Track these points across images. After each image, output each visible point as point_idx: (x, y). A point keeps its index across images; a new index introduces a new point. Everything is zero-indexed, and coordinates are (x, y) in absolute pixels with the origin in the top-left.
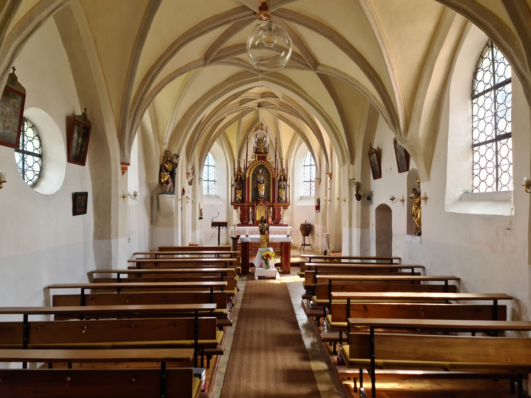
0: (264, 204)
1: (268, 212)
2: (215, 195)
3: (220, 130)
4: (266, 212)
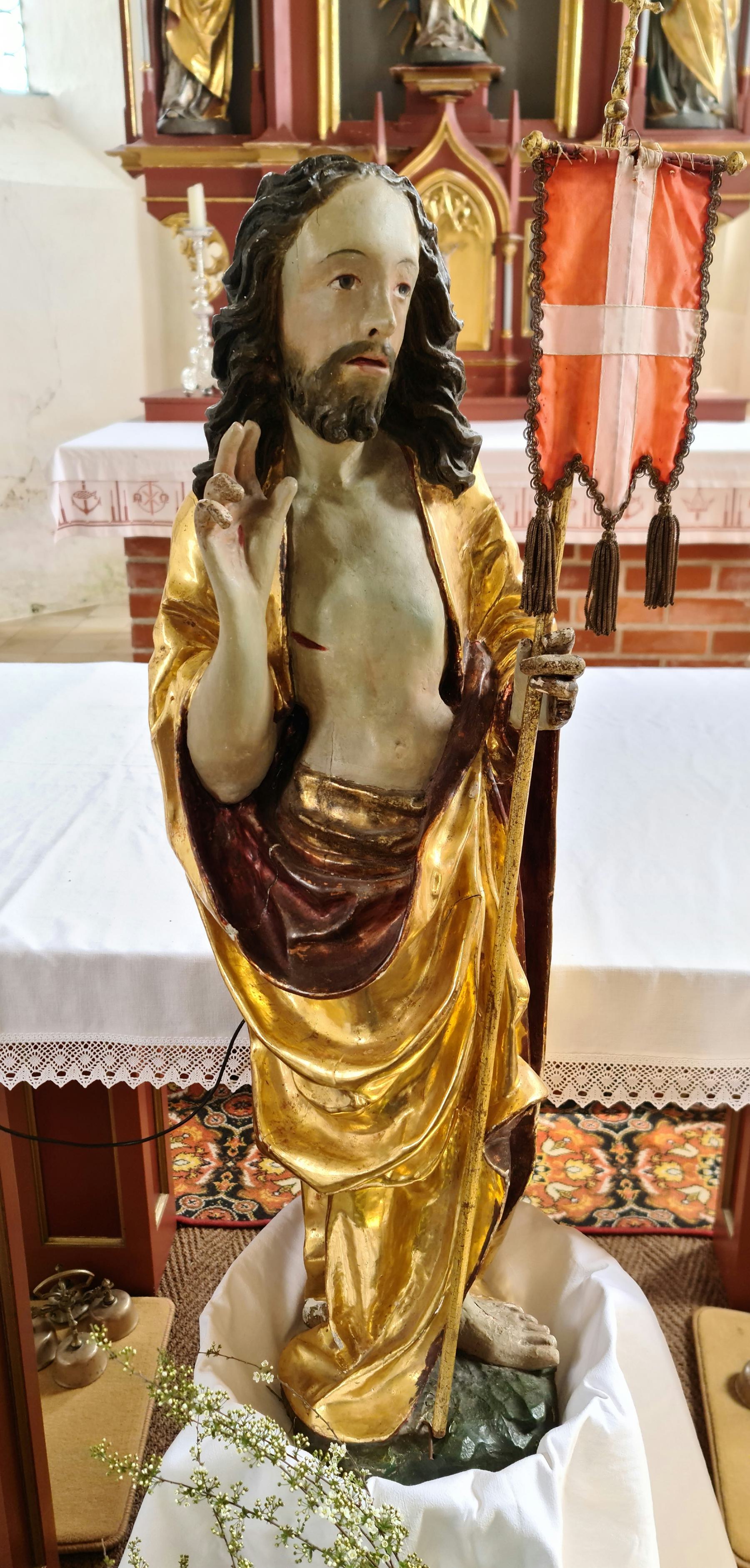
0: (487, 153)
1: (520, 245)
2: (34, 93)
3: (420, 1048)
4: (498, 248)
